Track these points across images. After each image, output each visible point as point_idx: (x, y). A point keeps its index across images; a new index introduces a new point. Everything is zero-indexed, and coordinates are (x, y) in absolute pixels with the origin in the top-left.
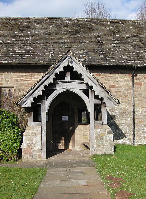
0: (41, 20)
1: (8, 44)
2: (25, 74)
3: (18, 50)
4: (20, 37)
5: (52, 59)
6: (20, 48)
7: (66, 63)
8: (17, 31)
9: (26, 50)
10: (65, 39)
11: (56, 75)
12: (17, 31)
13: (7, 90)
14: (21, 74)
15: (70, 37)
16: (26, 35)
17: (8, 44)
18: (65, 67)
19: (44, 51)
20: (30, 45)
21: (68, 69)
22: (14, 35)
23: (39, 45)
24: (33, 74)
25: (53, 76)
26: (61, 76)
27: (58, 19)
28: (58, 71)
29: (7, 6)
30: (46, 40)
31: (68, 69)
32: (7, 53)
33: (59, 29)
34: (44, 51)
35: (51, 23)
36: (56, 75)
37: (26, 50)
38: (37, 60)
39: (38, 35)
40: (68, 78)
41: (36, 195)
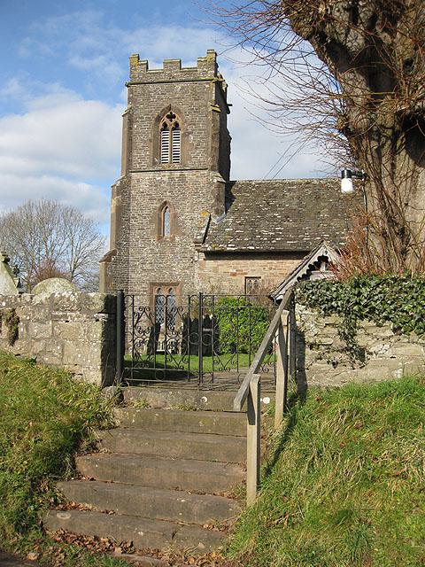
0: (293, 184)
1: (252, 224)
2: (275, 262)
3: (265, 232)
4: (266, 212)
5: (307, 243)
6: (268, 228)
7: (320, 253)
8: (261, 202)
9: (275, 231)
10: (324, 214)
11: (310, 266)
12: (261, 202)
13: (253, 281)
14: (270, 261)
15: (329, 212)
16: (274, 209)
17: (252, 224)
18: (319, 258)
19: (298, 231)
20: (280, 223)
21: (323, 259)
22: (259, 210)
23: (290, 224)
24: (284, 261)
25: (307, 267)
26: (316, 266)
27: (315, 182)
28: (311, 262)
29: (30, 206)
30: (299, 215)
31: (323, 259)
32: (253, 235)
33: (318, 198)
34: (298, 231)
35: (306, 188)
36: (310, 266)
37: (275, 231)
38: (289, 245)
39: (290, 210)
40: (323, 269)
41: (329, 260)
